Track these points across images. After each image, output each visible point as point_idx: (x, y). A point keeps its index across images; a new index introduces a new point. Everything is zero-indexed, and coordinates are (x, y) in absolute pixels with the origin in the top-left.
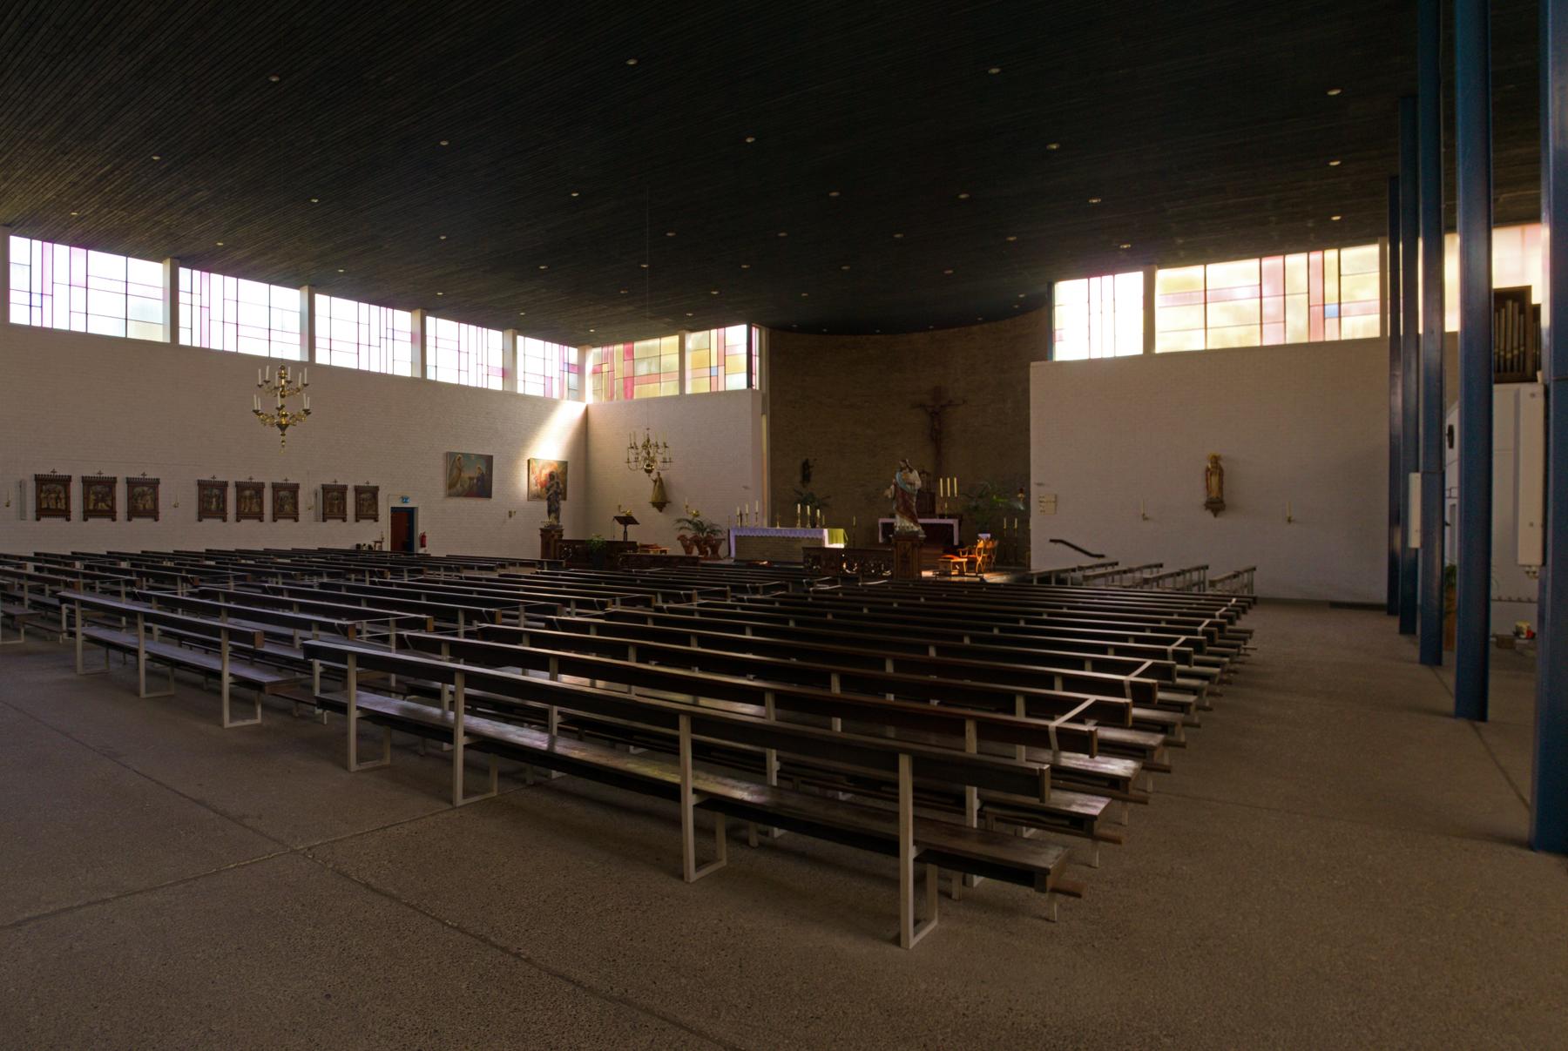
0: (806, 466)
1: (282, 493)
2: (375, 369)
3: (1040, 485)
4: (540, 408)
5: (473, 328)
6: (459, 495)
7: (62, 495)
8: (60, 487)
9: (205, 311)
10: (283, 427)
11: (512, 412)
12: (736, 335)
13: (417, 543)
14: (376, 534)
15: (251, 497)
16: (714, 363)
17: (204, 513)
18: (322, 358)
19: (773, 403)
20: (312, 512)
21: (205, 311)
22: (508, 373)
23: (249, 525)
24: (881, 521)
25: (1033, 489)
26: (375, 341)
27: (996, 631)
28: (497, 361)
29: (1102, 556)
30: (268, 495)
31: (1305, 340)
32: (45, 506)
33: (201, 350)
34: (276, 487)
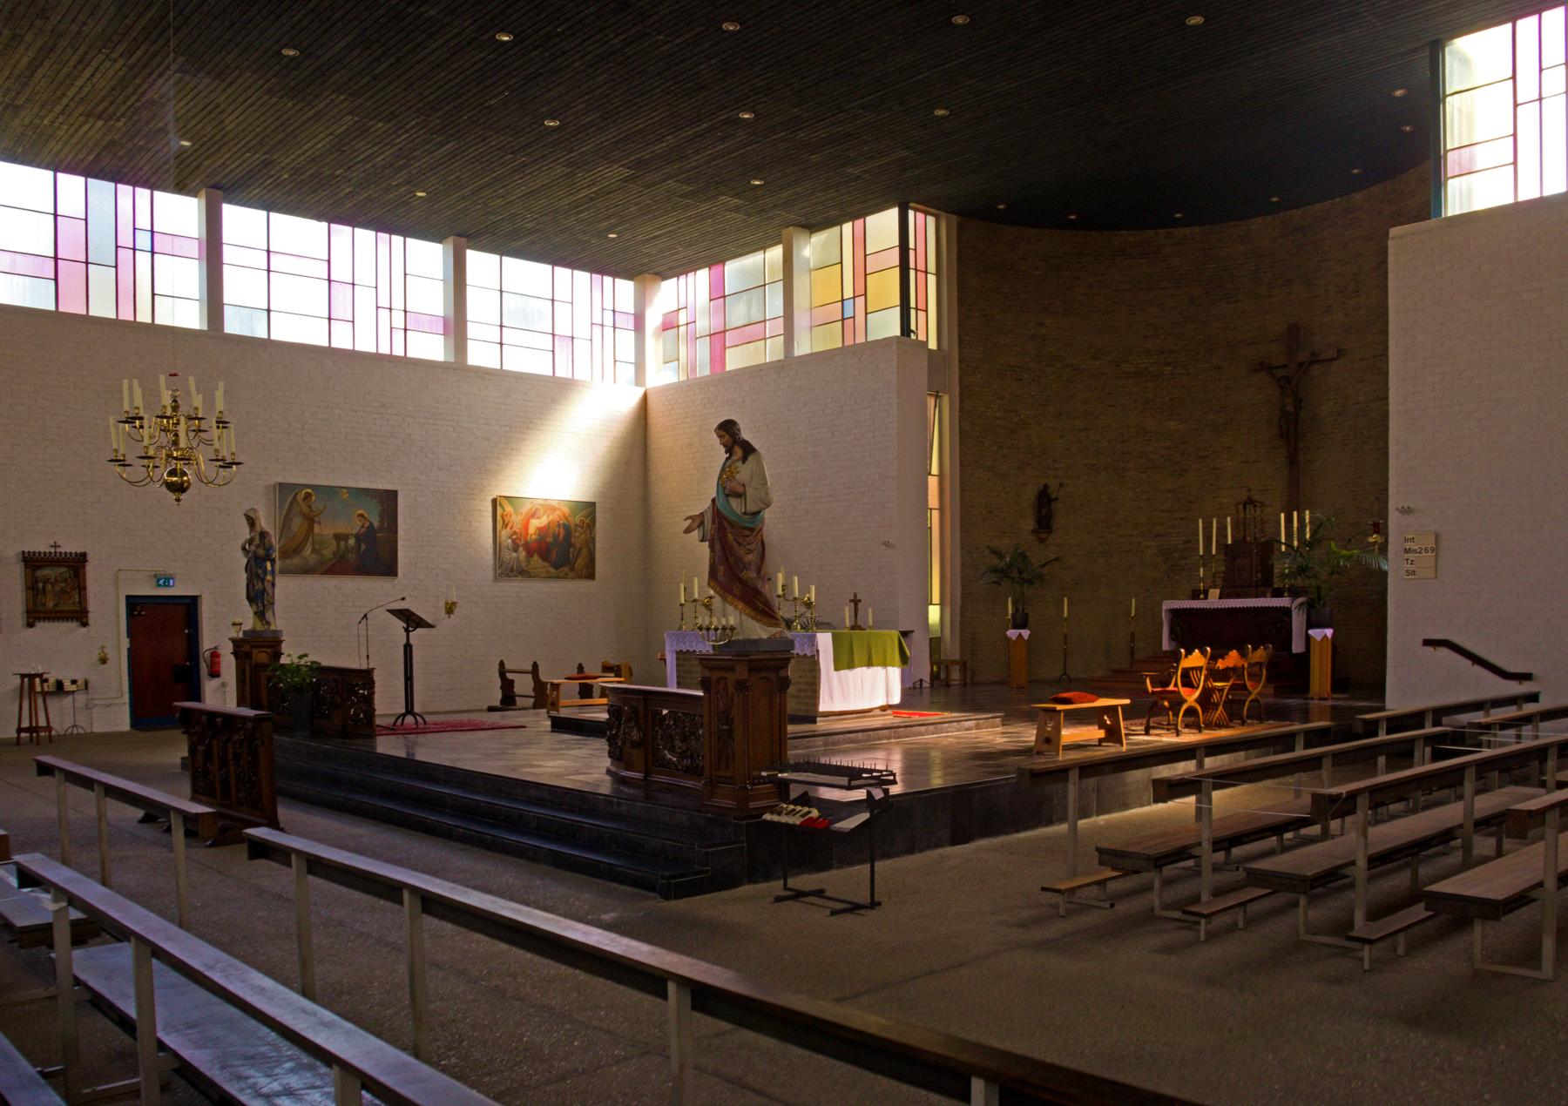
0: (1045, 500)
4: (528, 401)
6: (307, 570)
9: (384, 302)
12: (883, 225)
16: (848, 293)
21: (384, 302)
22: (456, 326)
24: (1168, 605)
25: (1394, 519)
26: (582, 331)
28: (431, 298)
29: (1526, 677)
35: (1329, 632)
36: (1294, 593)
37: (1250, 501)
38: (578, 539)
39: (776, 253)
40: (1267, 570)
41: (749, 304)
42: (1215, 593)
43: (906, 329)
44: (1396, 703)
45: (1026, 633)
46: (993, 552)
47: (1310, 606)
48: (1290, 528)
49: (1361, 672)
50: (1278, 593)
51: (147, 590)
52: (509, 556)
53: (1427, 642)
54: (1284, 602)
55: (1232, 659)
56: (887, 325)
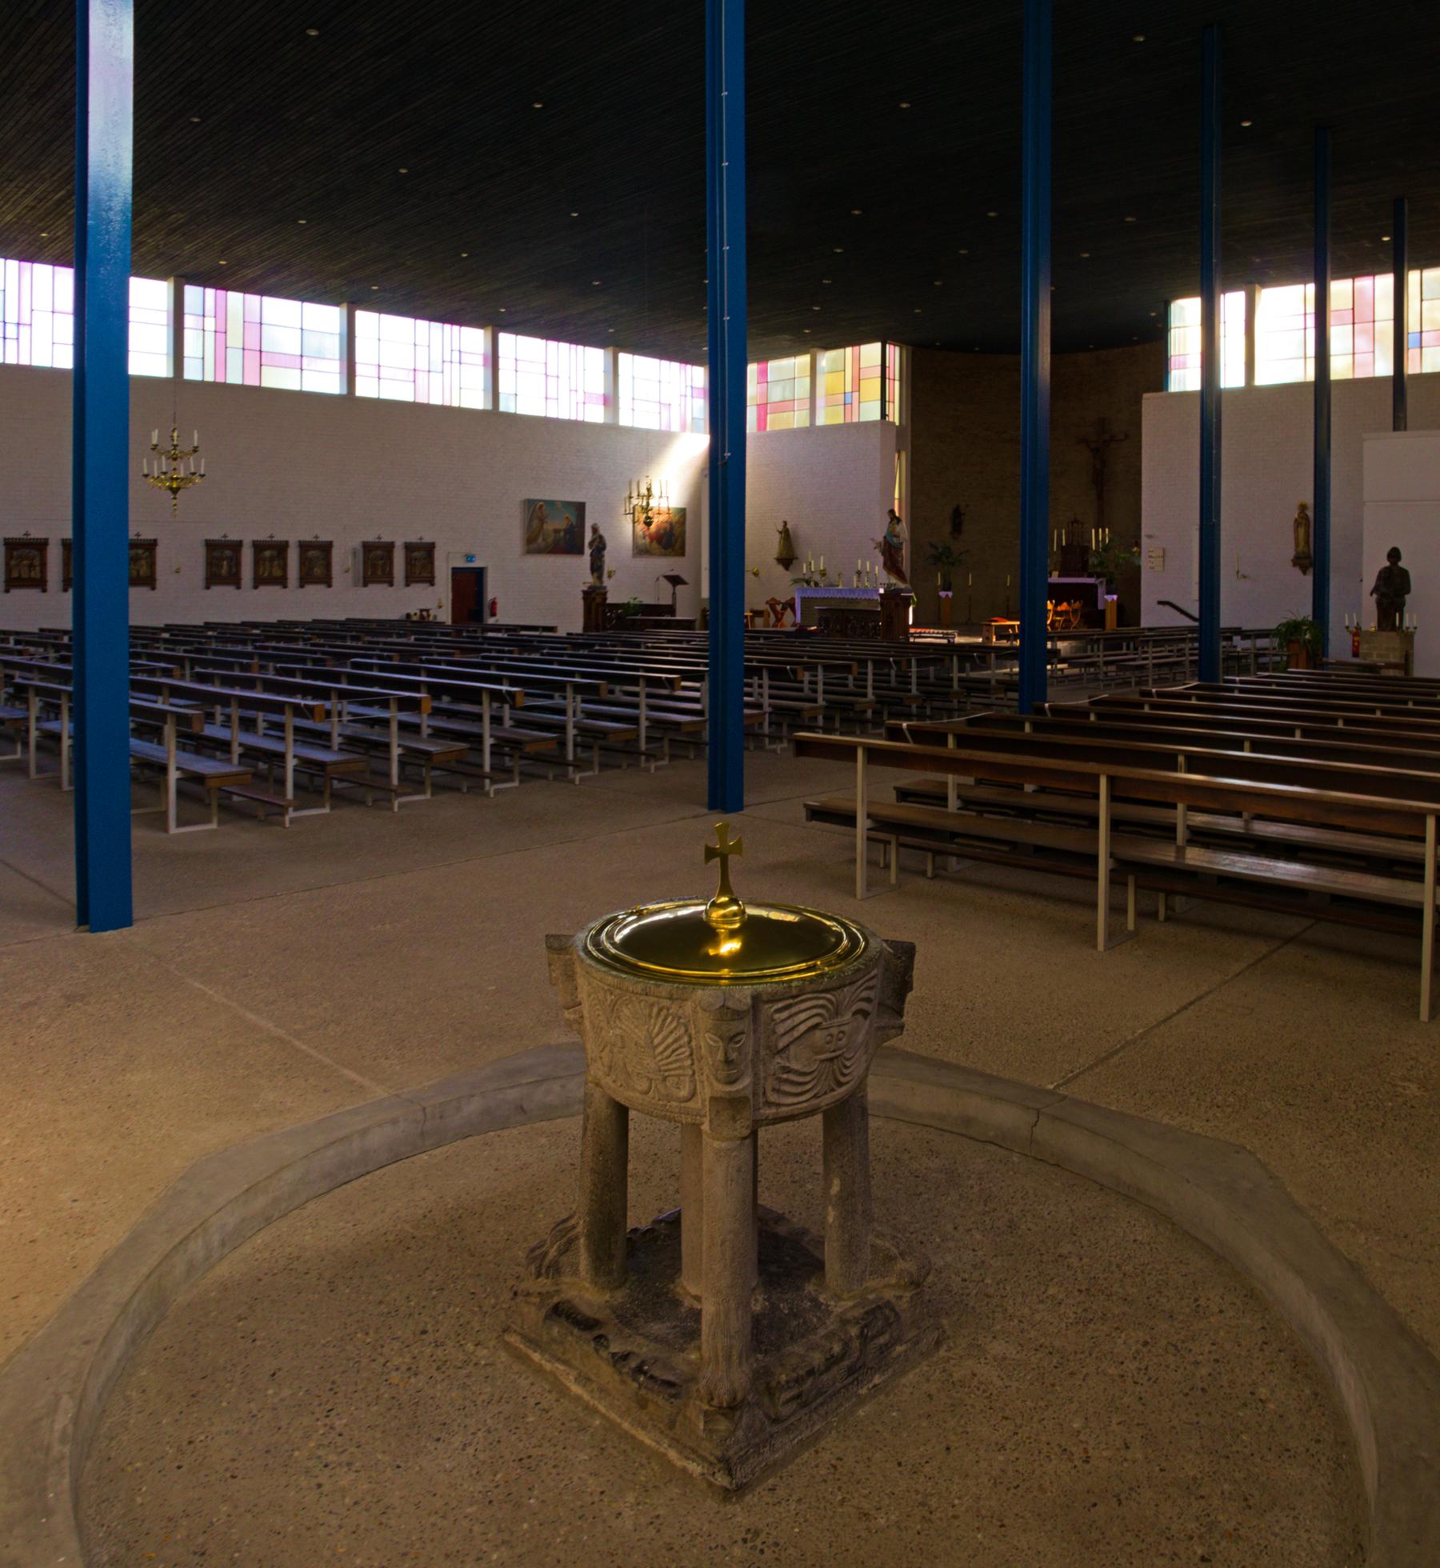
1: (311, 553)
2: (436, 400)
3: (1150, 537)
4: (652, 443)
5: (564, 346)
7: (37, 562)
8: (34, 552)
10: (175, 491)
11: (611, 447)
12: (871, 352)
13: (487, 610)
14: (435, 601)
15: (272, 559)
16: (849, 389)
17: (213, 579)
18: (365, 388)
19: (915, 435)
20: (350, 575)
22: (611, 400)
23: (377, 590)
25: (1144, 541)
27: (1147, 709)
30: (293, 557)
31: (1350, 376)
32: (15, 575)
33: (214, 385)
34: (304, 547)
35: (1115, 597)
36: (1099, 576)
37: (1076, 521)
38: (677, 531)
39: (805, 359)
40: (1085, 563)
41: (784, 388)
42: (1055, 574)
43: (884, 415)
44: (1143, 625)
45: (950, 594)
46: (931, 545)
47: (1110, 582)
48: (1098, 537)
49: (1129, 611)
50: (1090, 576)
51: (461, 564)
52: (641, 541)
53: (1160, 603)
54: (1091, 580)
55: (1064, 607)
56: (871, 412)
